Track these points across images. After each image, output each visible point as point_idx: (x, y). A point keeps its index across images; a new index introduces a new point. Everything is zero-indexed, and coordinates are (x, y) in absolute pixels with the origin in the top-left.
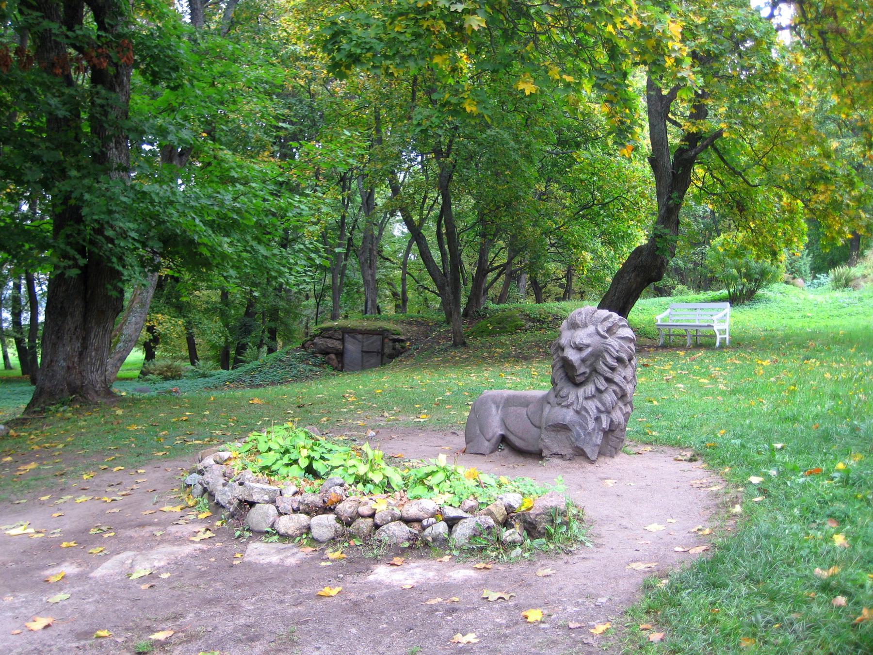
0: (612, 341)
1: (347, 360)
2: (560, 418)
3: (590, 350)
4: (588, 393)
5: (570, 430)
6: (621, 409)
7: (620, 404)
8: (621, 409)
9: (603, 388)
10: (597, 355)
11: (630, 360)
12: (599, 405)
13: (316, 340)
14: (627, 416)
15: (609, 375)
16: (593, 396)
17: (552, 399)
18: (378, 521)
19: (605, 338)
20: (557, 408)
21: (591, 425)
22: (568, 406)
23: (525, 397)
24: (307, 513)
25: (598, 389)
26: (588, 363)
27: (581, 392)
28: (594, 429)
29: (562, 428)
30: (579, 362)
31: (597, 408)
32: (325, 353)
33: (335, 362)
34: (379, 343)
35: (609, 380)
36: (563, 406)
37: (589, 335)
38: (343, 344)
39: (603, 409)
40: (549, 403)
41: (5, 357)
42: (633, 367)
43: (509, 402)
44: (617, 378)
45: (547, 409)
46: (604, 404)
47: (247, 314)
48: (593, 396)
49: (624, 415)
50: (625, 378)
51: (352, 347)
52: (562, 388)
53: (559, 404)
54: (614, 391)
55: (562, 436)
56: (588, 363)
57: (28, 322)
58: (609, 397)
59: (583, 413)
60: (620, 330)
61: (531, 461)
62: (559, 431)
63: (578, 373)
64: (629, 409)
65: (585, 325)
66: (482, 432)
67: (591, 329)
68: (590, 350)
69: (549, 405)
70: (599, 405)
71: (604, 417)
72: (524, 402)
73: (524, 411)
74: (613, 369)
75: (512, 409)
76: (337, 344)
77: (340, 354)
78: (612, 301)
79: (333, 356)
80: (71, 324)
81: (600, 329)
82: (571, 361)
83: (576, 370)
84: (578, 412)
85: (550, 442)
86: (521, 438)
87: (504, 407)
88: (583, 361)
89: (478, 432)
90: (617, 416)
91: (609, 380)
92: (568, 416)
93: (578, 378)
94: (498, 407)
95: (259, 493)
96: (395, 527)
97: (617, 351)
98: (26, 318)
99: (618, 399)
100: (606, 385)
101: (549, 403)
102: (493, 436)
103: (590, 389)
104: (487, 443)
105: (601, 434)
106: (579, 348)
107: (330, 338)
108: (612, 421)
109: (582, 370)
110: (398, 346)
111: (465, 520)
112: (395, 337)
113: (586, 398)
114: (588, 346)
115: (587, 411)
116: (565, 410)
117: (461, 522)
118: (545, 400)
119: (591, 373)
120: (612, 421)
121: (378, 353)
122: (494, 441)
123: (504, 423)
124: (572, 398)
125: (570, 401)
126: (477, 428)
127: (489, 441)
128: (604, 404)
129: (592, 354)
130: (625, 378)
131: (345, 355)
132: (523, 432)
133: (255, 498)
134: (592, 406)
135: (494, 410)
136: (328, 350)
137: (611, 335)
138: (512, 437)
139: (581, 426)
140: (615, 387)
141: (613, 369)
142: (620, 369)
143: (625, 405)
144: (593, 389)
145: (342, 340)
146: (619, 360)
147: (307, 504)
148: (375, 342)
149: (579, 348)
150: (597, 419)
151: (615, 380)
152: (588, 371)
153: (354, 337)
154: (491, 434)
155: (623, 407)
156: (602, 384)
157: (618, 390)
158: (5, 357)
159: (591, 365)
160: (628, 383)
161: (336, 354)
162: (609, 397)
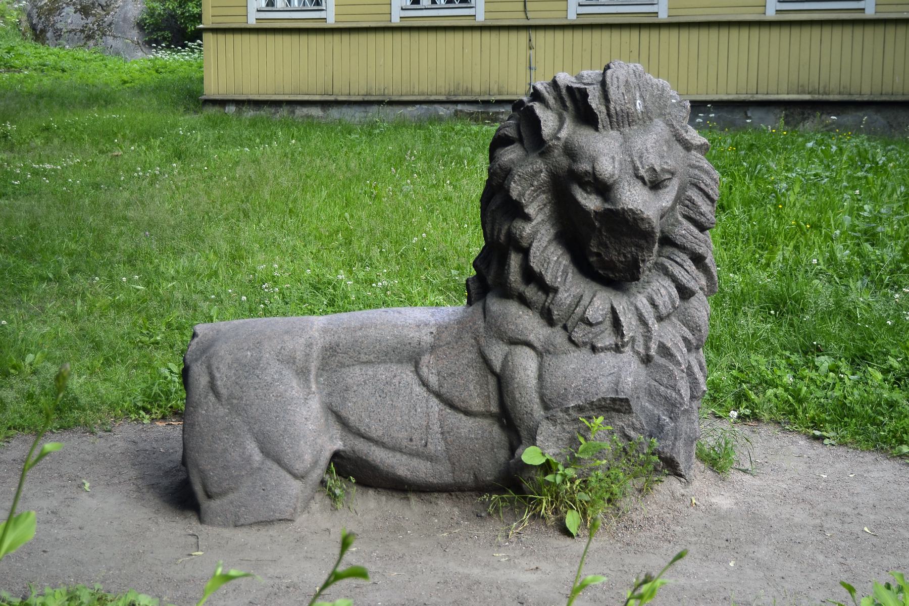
12: (690, 336)
59: (659, 360)
75: (356, 374)
84: (647, 360)
87: (324, 367)
89: (257, 457)
94: (302, 373)
102: (315, 463)
116: (608, 360)
135: (293, 387)
138: (379, 456)
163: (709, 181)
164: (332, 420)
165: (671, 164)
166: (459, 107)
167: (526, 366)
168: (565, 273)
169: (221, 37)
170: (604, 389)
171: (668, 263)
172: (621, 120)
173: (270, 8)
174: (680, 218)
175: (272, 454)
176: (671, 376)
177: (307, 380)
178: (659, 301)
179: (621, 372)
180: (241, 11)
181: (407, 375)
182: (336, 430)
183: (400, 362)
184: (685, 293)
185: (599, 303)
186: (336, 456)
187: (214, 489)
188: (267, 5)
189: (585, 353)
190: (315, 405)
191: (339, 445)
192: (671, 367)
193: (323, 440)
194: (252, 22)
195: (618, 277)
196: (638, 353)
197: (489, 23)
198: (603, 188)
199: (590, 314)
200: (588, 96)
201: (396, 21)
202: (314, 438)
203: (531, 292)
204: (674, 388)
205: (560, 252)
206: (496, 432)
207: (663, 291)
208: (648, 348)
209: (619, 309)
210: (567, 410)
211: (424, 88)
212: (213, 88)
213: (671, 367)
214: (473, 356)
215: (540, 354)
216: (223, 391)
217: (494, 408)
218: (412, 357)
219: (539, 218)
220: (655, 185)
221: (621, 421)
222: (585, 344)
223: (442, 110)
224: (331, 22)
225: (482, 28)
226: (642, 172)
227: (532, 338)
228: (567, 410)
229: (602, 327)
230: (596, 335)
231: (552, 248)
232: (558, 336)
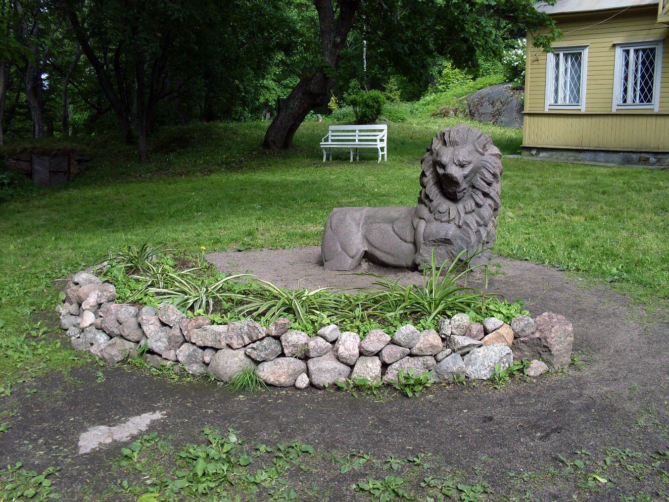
4: (469, 209)
5: (452, 244)
12: (479, 220)
15: (486, 189)
30: (462, 178)
31: (477, 222)
35: (486, 195)
38: (31, 165)
39: (482, 223)
46: (482, 218)
54: (490, 205)
55: (442, 250)
59: (465, 227)
61: (57, 228)
66: (344, 249)
70: (479, 220)
71: (482, 229)
74: (489, 184)
82: (456, 178)
84: (459, 227)
86: (389, 254)
87: (365, 223)
89: (340, 249)
91: (486, 195)
102: (357, 253)
104: (350, 261)
113: (466, 213)
114: (470, 163)
115: (468, 225)
122: (358, 257)
123: (366, 238)
126: (339, 245)
134: (472, 219)
135: (354, 229)
138: (378, 254)
139: (462, 239)
141: (489, 184)
145: (31, 162)
146: (494, 175)
151: (491, 195)
156: (480, 198)
163: (490, 166)
164: (365, 241)
165: (468, 159)
166: (642, 155)
167: (422, 225)
168: (437, 195)
169: (532, 118)
170: (442, 235)
171: (475, 196)
172: (454, 144)
173: (624, 104)
174: (479, 178)
175: (344, 249)
176: (469, 233)
177: (359, 226)
178: (467, 207)
179: (451, 231)
180: (542, 105)
181: (389, 228)
182: (366, 244)
183: (388, 223)
184: (478, 205)
185: (445, 205)
186: (366, 252)
187: (327, 259)
188: (623, 102)
189: (439, 222)
190: (360, 234)
191: (366, 249)
192: (469, 230)
193: (360, 246)
194: (547, 111)
195: (453, 198)
196: (455, 224)
197: (660, 113)
198: (443, 167)
199: (440, 209)
200: (208, 121)
201: (614, 111)
202: (358, 245)
203: (426, 201)
204: (469, 238)
205: (436, 188)
206: (411, 246)
207: (469, 204)
208: (459, 222)
209: (451, 208)
210: (429, 241)
211: (652, 145)
212: (526, 143)
213: (469, 230)
214: (410, 222)
215: (427, 222)
216: (333, 228)
217: (413, 240)
218: (392, 221)
219: (430, 176)
220: (462, 166)
221: (450, 247)
222: (439, 219)
223: (634, 156)
224: (583, 111)
225: (657, 115)
226: (455, 161)
227: (425, 217)
228: (429, 241)
229: (445, 214)
230: (442, 217)
231: (433, 187)
232: (431, 216)
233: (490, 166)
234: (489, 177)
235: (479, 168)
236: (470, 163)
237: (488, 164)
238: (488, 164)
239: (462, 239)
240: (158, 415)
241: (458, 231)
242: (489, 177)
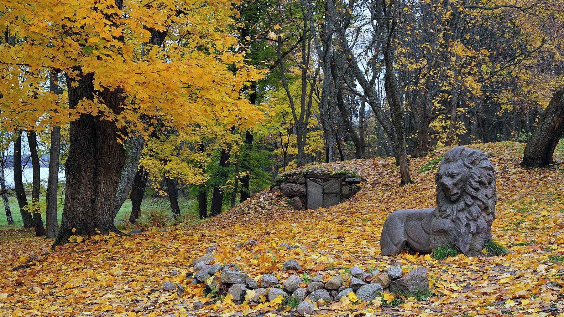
0: (475, 170)
1: (309, 202)
2: (442, 226)
3: (459, 177)
6: (484, 217)
7: (484, 214)
8: (484, 217)
9: (470, 204)
10: (465, 180)
11: (490, 183)
13: (283, 185)
14: (490, 223)
16: (464, 209)
17: (437, 214)
18: (309, 290)
19: (470, 168)
20: (440, 219)
21: (463, 230)
22: (446, 217)
23: (420, 213)
24: (265, 288)
25: (467, 205)
26: (459, 186)
27: (455, 207)
28: (465, 232)
29: (443, 232)
30: (452, 185)
32: (291, 196)
33: (300, 204)
34: (337, 185)
35: (474, 198)
36: (443, 218)
37: (459, 167)
39: (471, 218)
40: (435, 216)
41: (8, 213)
42: (492, 188)
43: (409, 218)
44: (480, 196)
45: (434, 221)
46: (471, 215)
47: (222, 164)
48: (464, 209)
49: (487, 222)
50: (486, 195)
51: (315, 190)
52: (443, 205)
53: (441, 216)
54: (479, 205)
56: (459, 186)
57: (31, 180)
58: (475, 210)
59: (457, 221)
60: (481, 162)
62: (442, 235)
63: (452, 194)
64: (491, 217)
65: (456, 161)
67: (460, 163)
68: (459, 177)
69: (435, 218)
70: (468, 215)
72: (420, 217)
73: (419, 223)
74: (477, 190)
76: (301, 188)
77: (304, 197)
78: (539, 139)
79: (297, 198)
80: (86, 178)
81: (466, 162)
82: (446, 185)
83: (450, 192)
84: (453, 221)
85: (436, 242)
86: (417, 243)
88: (455, 185)
89: (389, 240)
90: (482, 222)
91: (474, 198)
92: (447, 224)
93: (452, 197)
94: (402, 222)
95: (234, 277)
96: (320, 293)
97: (479, 177)
98: (28, 175)
99: (482, 211)
100: (473, 201)
101: (435, 216)
103: (461, 205)
105: (471, 235)
106: (452, 176)
107: (293, 182)
108: (478, 226)
109: (455, 191)
110: (354, 187)
111: (364, 286)
112: (351, 179)
113: (459, 211)
114: (458, 174)
115: (460, 221)
116: (444, 220)
117: (361, 287)
118: (433, 215)
119: (461, 193)
120: (478, 226)
121: (336, 194)
124: (449, 211)
125: (448, 214)
126: (388, 237)
127: (396, 246)
128: (471, 215)
129: (461, 180)
130: (486, 195)
131: (308, 197)
132: (419, 237)
133: (232, 280)
134: (463, 216)
135: (399, 223)
136: (293, 193)
137: (475, 166)
138: (412, 242)
140: (479, 202)
141: (477, 190)
142: (482, 189)
143: (488, 215)
144: (464, 204)
145: (305, 184)
146: (481, 183)
147: (265, 282)
148: (334, 186)
149: (452, 176)
150: (467, 225)
151: (479, 197)
152: (459, 191)
153: (315, 181)
154: (397, 242)
155: (486, 216)
156: (469, 201)
157: (481, 204)
158: (8, 213)
159: (462, 187)
160: (489, 199)
161: (300, 197)
162: (475, 210)
163: (476, 176)
233: (476, 176)
234: (477, 185)
235: (468, 178)
236: (458, 174)
237: (474, 175)
238: (474, 175)
239: (455, 229)
240: (59, 223)
241: (453, 225)
242: (477, 185)
